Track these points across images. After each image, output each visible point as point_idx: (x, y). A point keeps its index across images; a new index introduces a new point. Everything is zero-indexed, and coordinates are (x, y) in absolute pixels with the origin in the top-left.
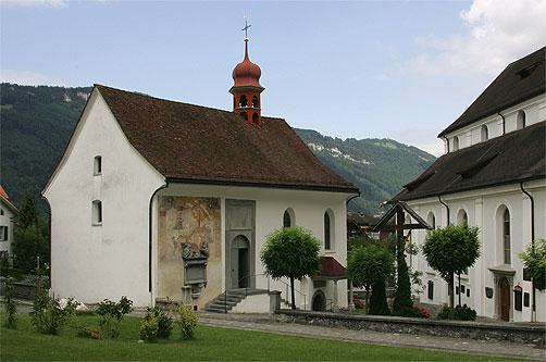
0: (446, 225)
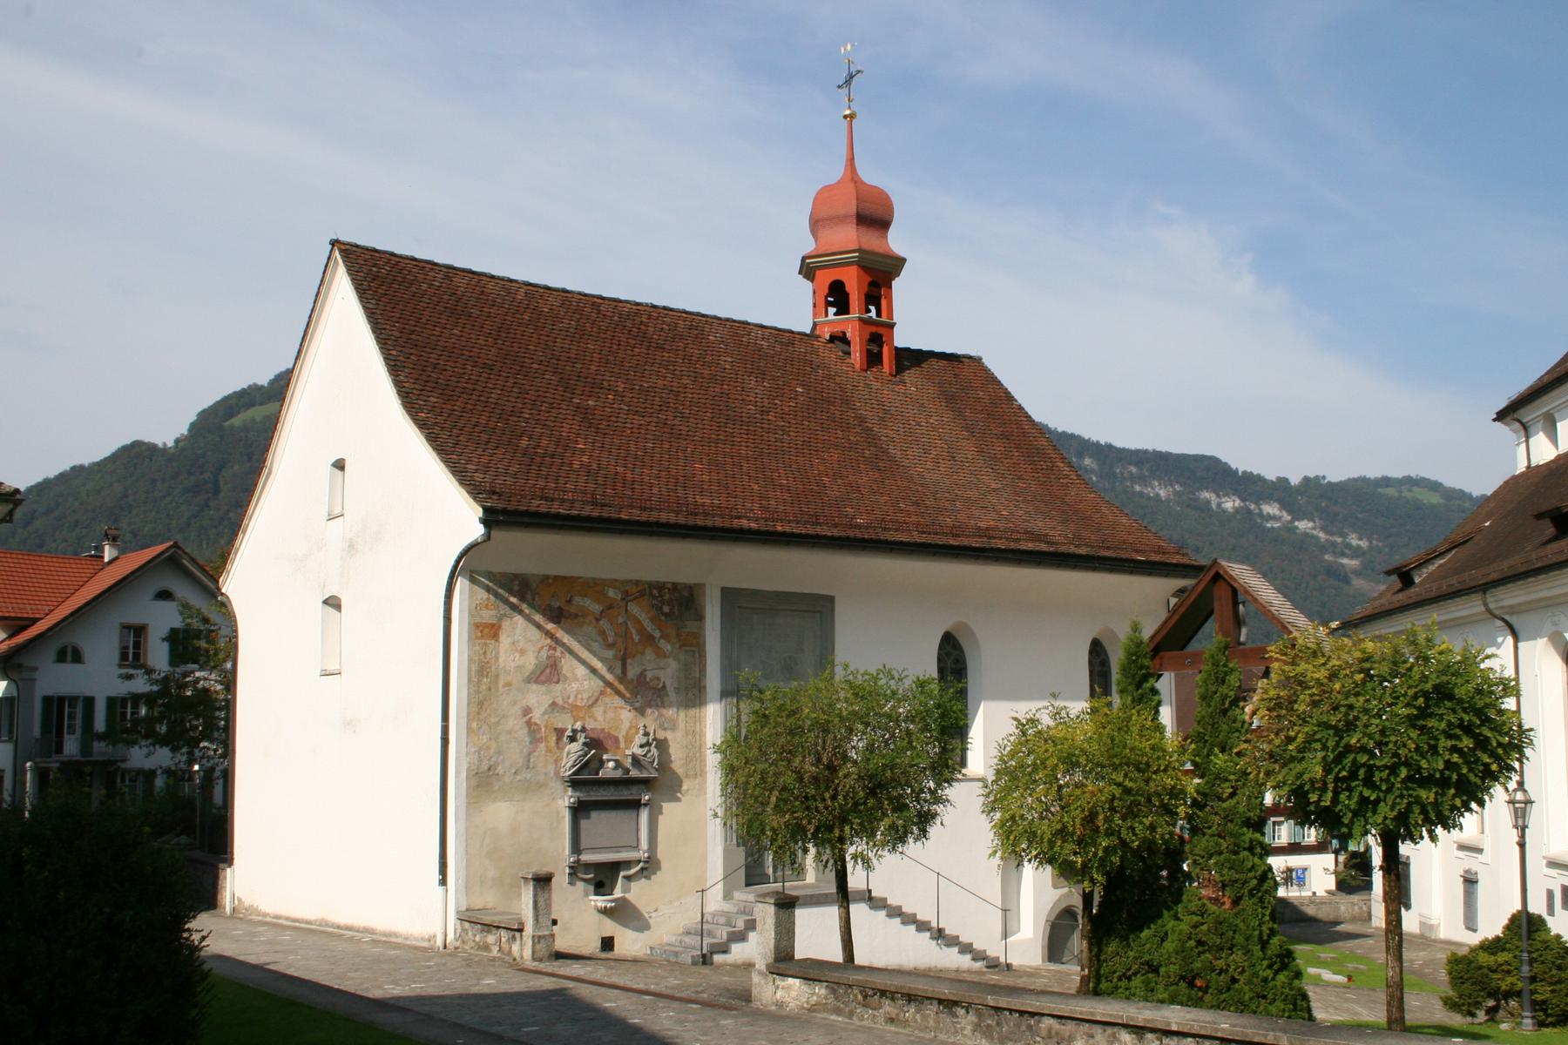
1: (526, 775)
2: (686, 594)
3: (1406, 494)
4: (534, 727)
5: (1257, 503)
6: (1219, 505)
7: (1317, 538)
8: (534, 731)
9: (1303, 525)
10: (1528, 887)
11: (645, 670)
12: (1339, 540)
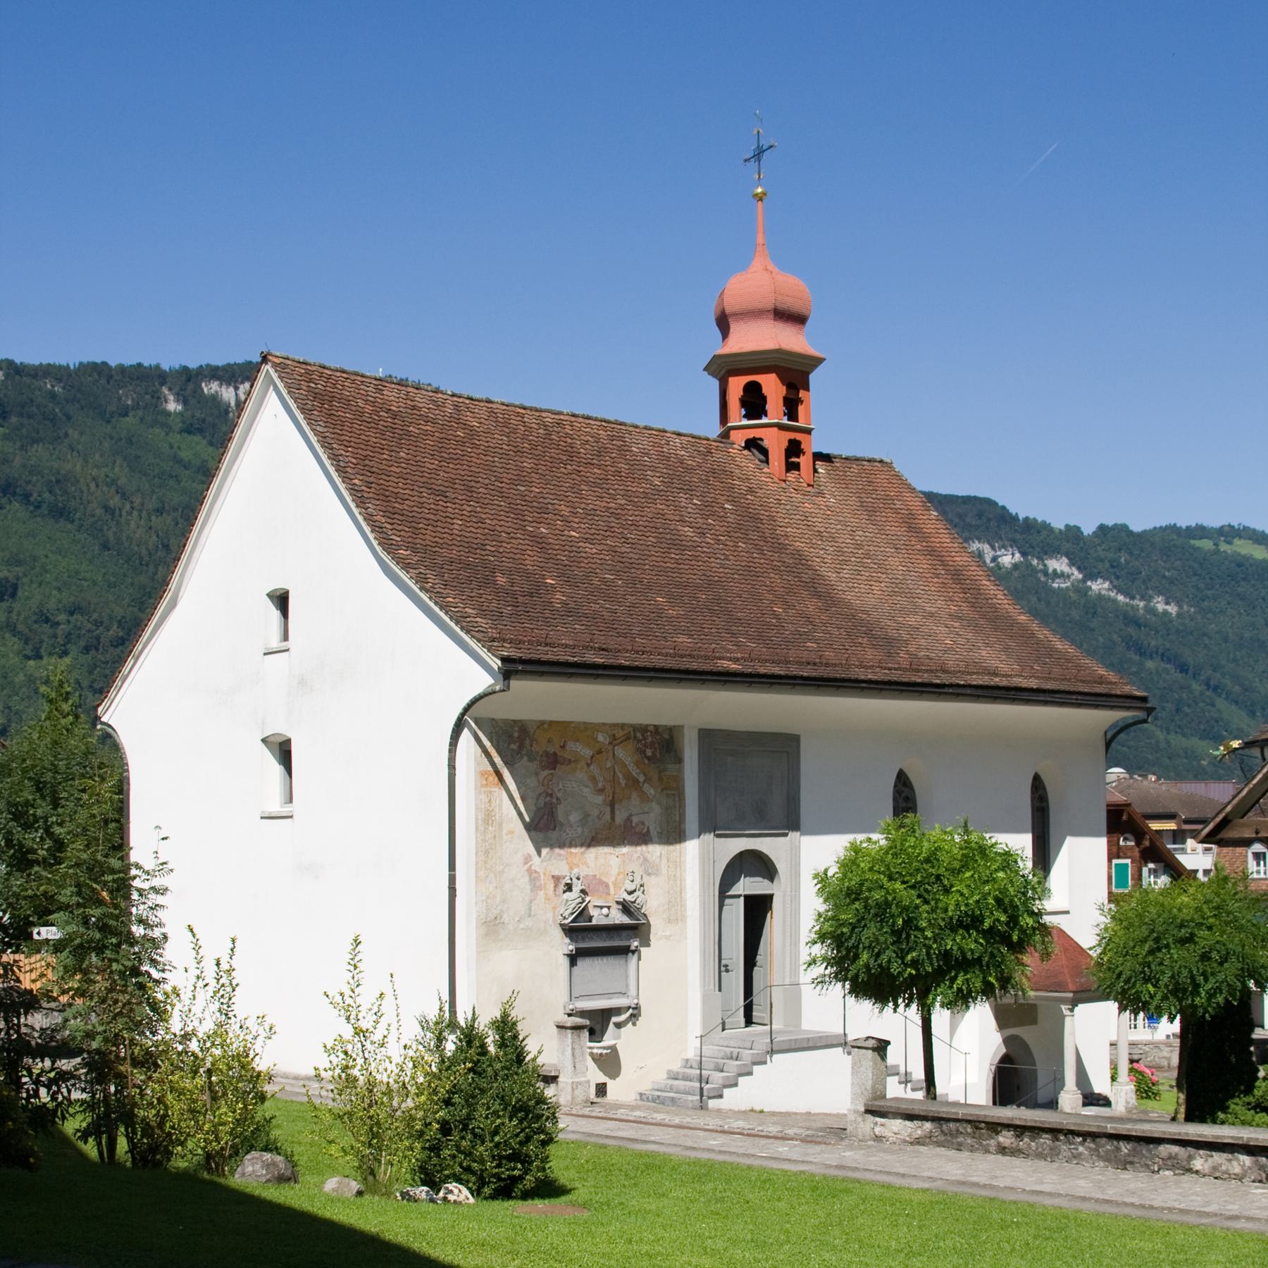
0: (569, 1098)
1: (528, 923)
2: (666, 736)
3: (1224, 547)
4: (534, 875)
5: (1040, 559)
6: (994, 559)
7: (1115, 601)
8: (535, 879)
9: (1099, 586)
10: (934, 1031)
11: (631, 815)
12: (1142, 604)
